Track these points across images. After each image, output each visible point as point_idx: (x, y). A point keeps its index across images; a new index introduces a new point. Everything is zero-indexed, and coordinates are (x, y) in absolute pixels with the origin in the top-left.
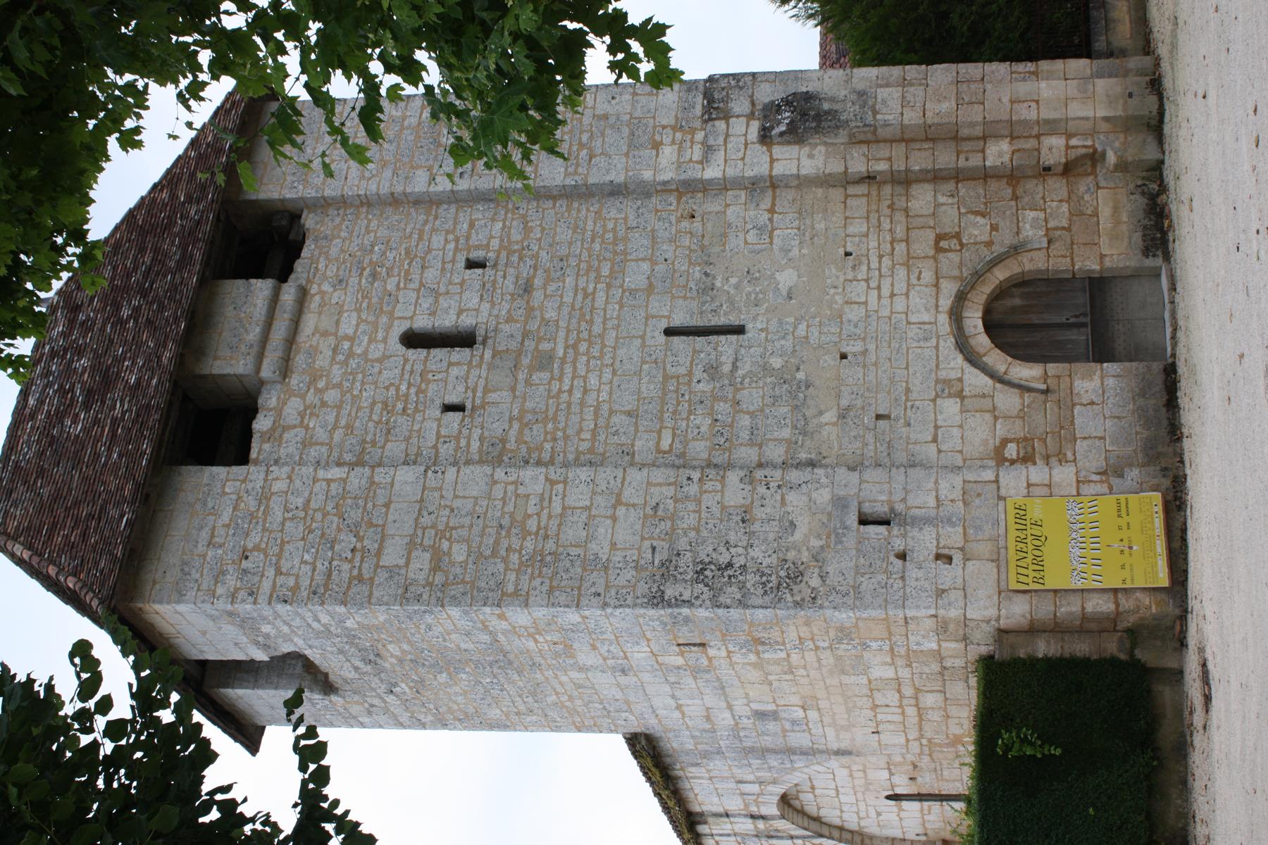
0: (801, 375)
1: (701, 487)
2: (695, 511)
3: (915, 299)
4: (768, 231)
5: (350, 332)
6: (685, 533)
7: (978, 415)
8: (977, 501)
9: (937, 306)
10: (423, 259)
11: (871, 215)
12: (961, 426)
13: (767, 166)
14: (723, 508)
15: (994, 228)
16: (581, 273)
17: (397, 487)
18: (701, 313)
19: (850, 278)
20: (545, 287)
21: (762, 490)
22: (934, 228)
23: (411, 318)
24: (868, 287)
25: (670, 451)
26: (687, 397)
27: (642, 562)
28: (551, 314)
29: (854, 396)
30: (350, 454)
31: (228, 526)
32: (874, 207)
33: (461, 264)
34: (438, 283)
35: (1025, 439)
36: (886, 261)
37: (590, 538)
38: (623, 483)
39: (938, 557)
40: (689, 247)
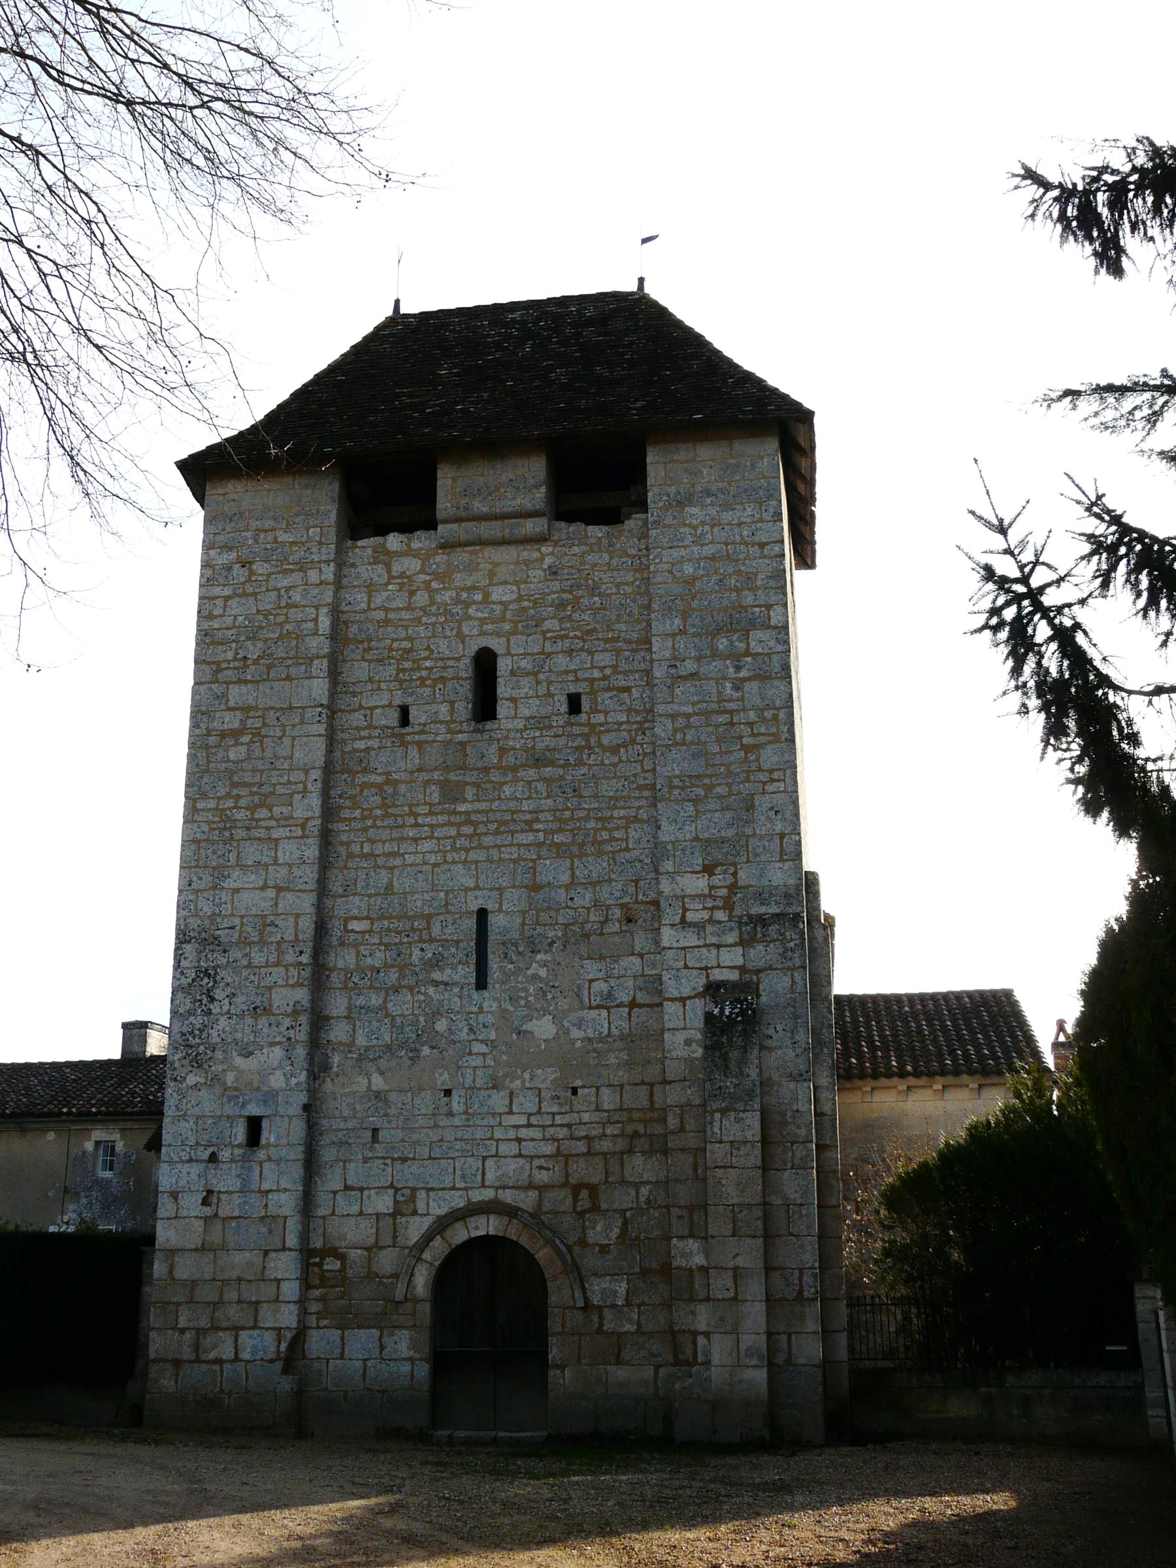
0: (426, 1051)
1: (291, 965)
2: (267, 961)
3: (512, 1165)
4: (607, 1003)
5: (494, 597)
6: (246, 955)
7: (374, 1231)
8: (264, 1230)
9: (504, 1187)
10: (582, 649)
11: (625, 1114)
12: (361, 1214)
13: (676, 994)
14: (270, 988)
15: (604, 1249)
16: (558, 814)
17: (307, 682)
18: (504, 943)
19: (543, 1094)
20: (541, 779)
21: (287, 1022)
22: (606, 1181)
23: (509, 653)
24: (530, 1115)
25: (346, 930)
26: (406, 940)
27: (219, 920)
28: (508, 790)
29: (399, 1105)
30: (357, 631)
31: (275, 540)
32: (636, 1115)
33: (572, 689)
34: (550, 671)
35: (345, 1278)
36: (562, 1133)
37: (244, 868)
38: (301, 891)
39: (210, 1192)
40: (588, 921)
